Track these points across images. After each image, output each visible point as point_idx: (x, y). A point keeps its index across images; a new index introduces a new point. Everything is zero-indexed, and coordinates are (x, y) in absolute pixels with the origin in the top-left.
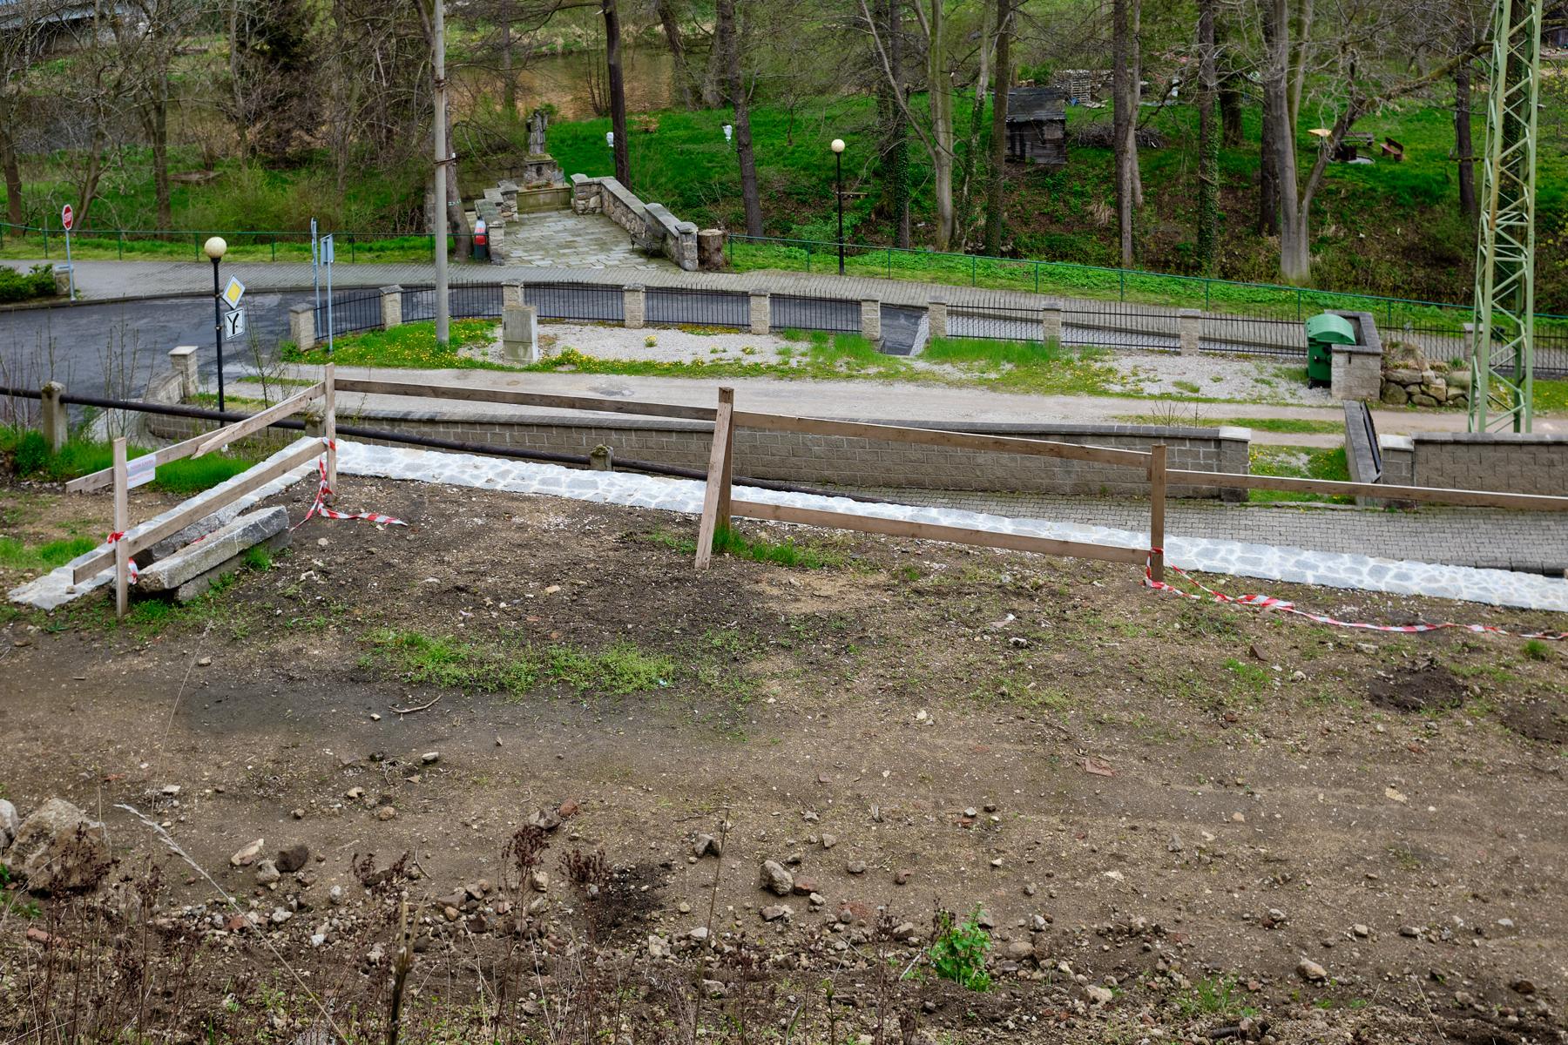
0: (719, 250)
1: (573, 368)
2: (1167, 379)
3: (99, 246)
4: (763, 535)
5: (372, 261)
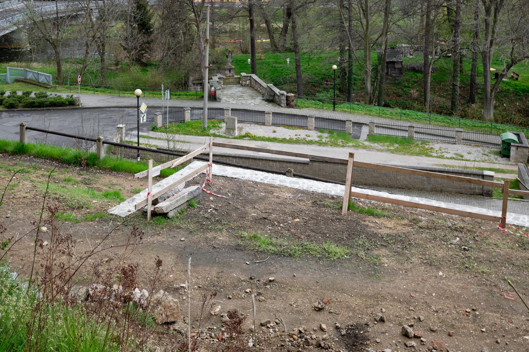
0: (293, 101)
1: (249, 138)
2: (452, 152)
3: (86, 89)
4: (361, 204)
5: (177, 99)
